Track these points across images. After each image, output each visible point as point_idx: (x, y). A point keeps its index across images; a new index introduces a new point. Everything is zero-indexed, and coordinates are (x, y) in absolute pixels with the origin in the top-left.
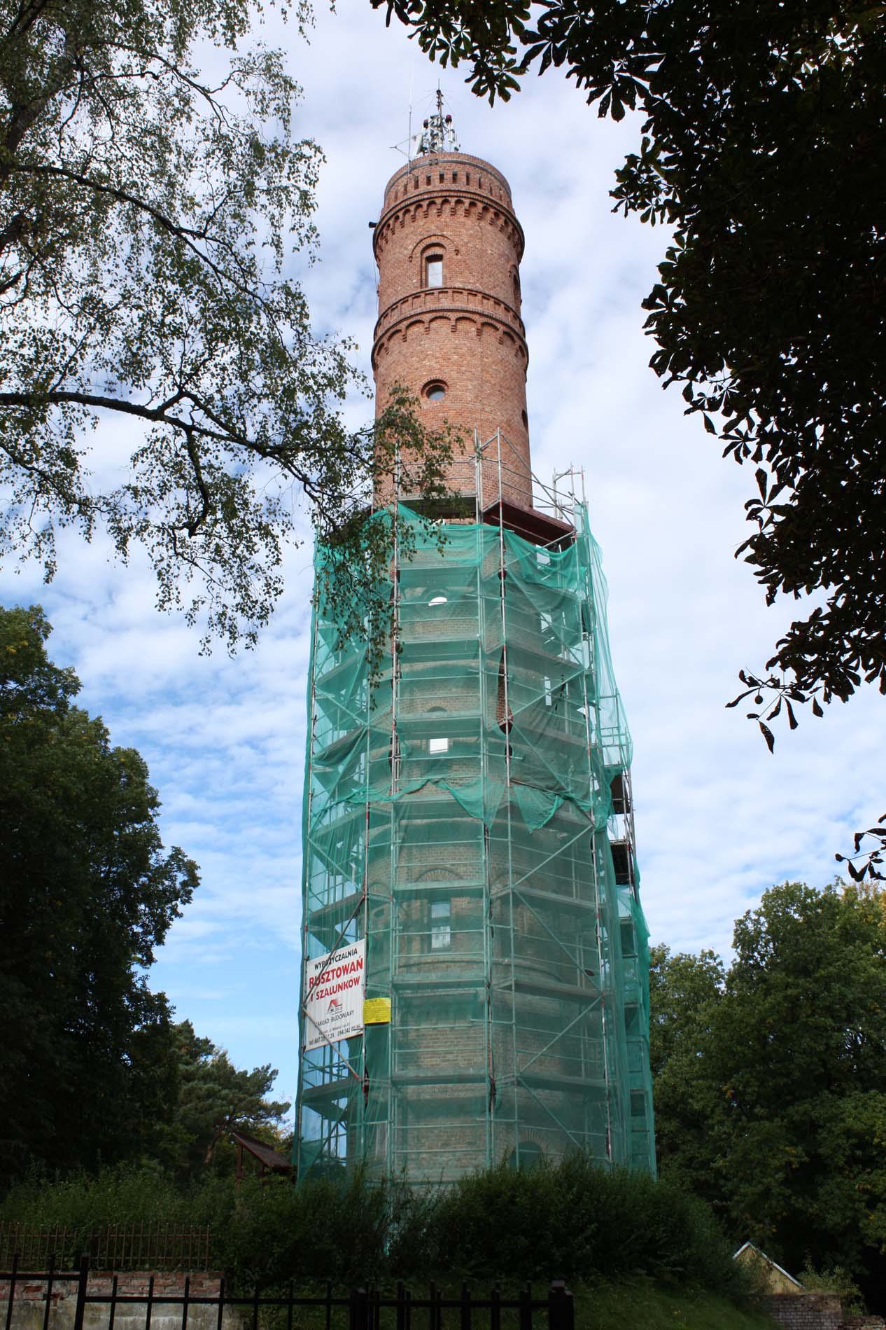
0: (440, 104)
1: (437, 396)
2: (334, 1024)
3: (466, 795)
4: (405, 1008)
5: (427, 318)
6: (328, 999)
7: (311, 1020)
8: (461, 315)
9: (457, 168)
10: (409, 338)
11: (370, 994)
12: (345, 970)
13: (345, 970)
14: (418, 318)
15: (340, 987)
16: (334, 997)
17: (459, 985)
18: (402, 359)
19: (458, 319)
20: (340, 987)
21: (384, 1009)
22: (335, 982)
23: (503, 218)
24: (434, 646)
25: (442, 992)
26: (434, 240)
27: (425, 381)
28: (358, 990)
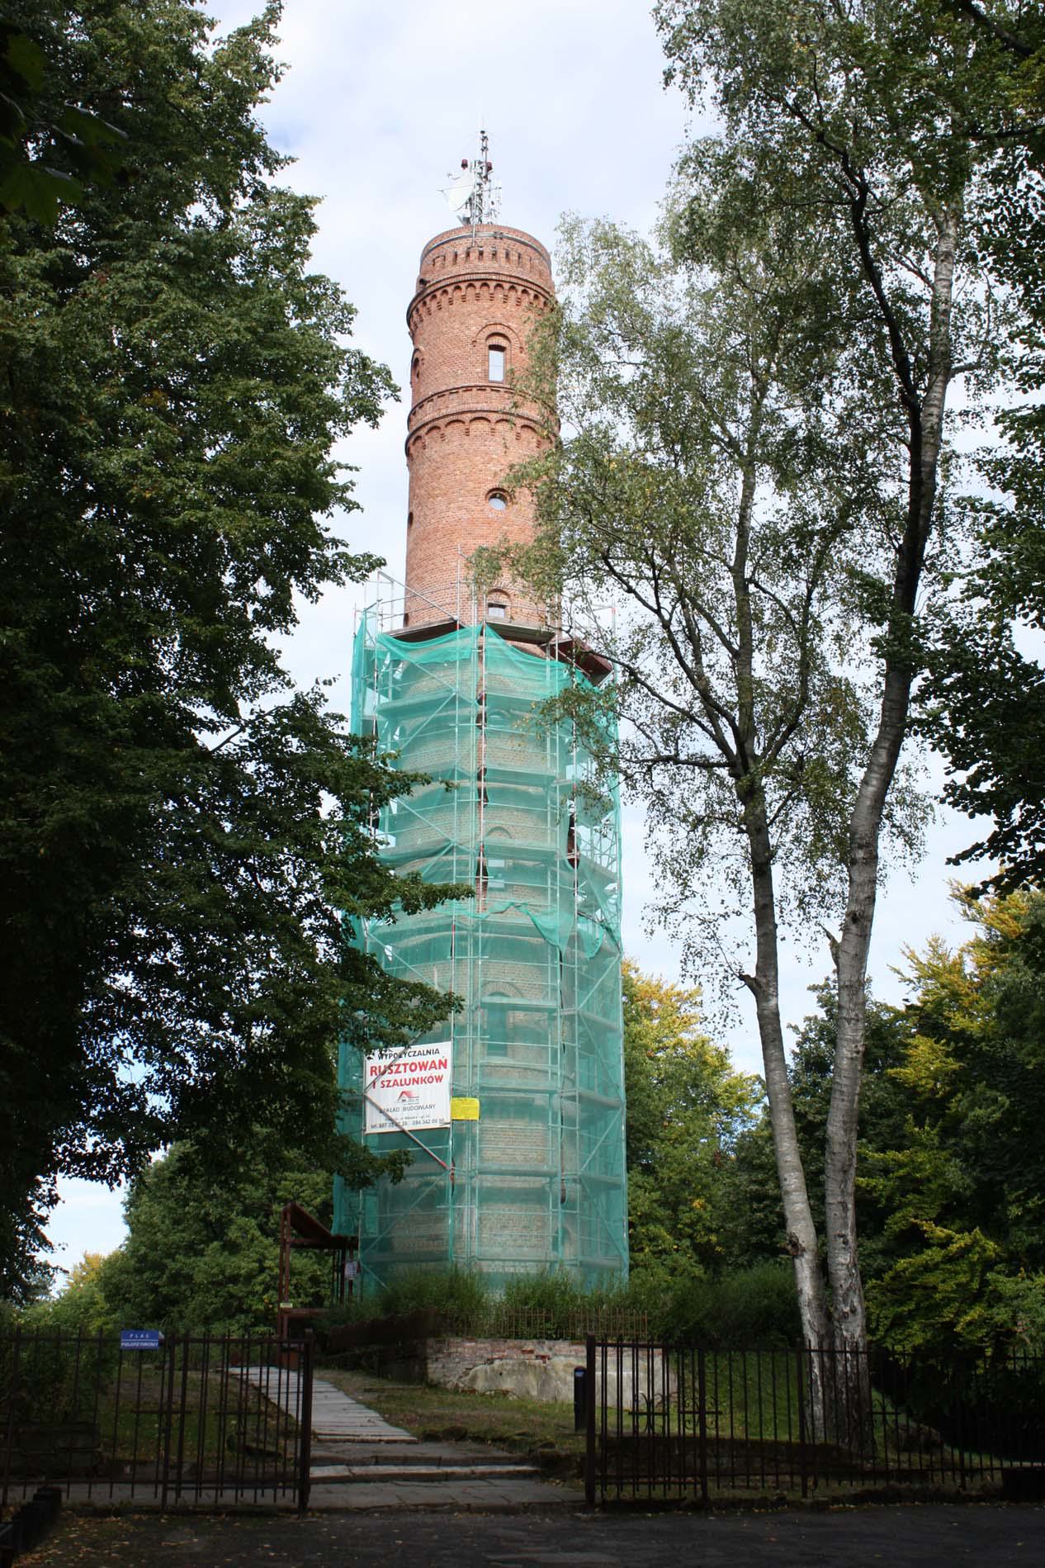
0: (484, 149)
1: (497, 504)
2: (406, 1114)
3: (545, 922)
4: (490, 1108)
5: (494, 417)
6: (398, 1090)
7: (373, 1104)
8: (527, 422)
9: (522, 249)
10: (472, 433)
11: (456, 1093)
12: (423, 1066)
13: (423, 1066)
14: (484, 415)
15: (416, 1081)
16: (406, 1088)
17: (502, 1089)
18: (463, 453)
19: (524, 426)
20: (416, 1081)
21: (471, 1109)
22: (409, 1075)
23: (542, 299)
24: (517, 774)
25: (502, 1094)
26: (499, 329)
27: (490, 486)
28: (444, 1087)
